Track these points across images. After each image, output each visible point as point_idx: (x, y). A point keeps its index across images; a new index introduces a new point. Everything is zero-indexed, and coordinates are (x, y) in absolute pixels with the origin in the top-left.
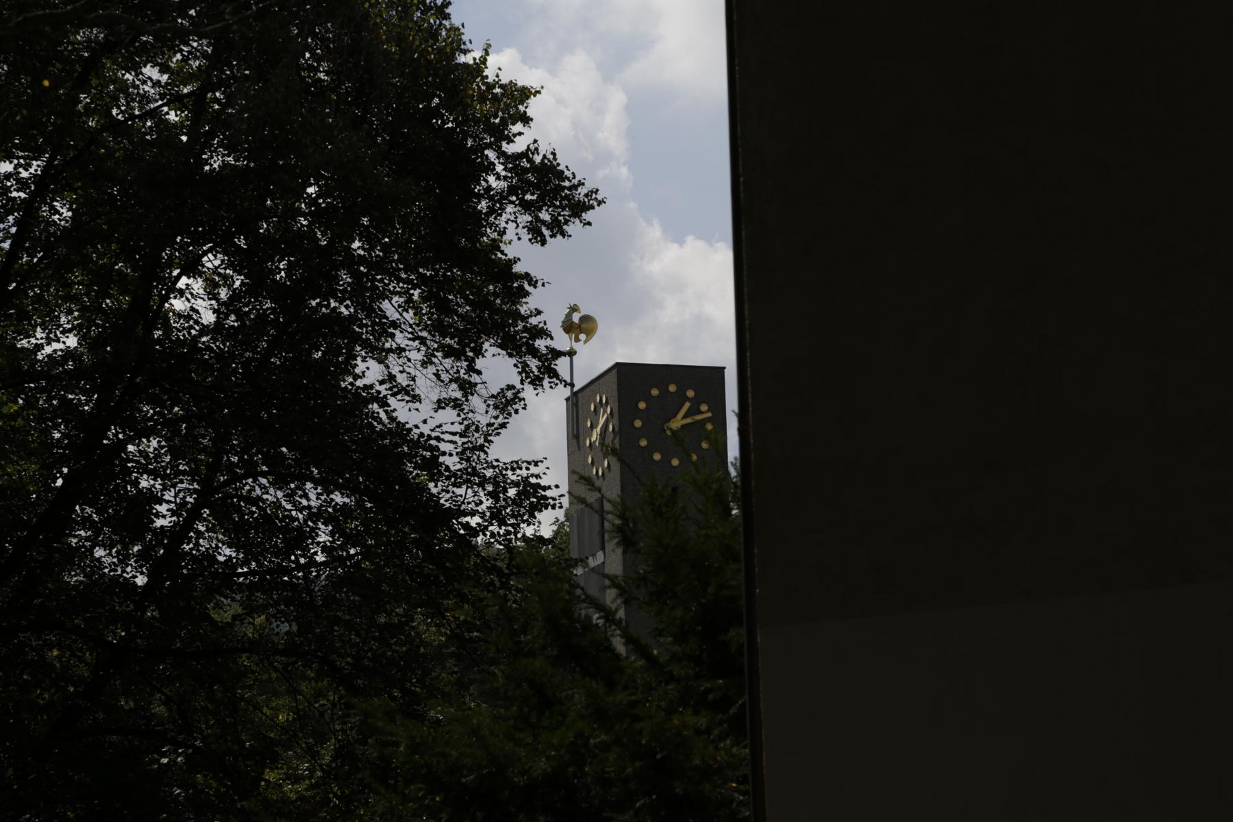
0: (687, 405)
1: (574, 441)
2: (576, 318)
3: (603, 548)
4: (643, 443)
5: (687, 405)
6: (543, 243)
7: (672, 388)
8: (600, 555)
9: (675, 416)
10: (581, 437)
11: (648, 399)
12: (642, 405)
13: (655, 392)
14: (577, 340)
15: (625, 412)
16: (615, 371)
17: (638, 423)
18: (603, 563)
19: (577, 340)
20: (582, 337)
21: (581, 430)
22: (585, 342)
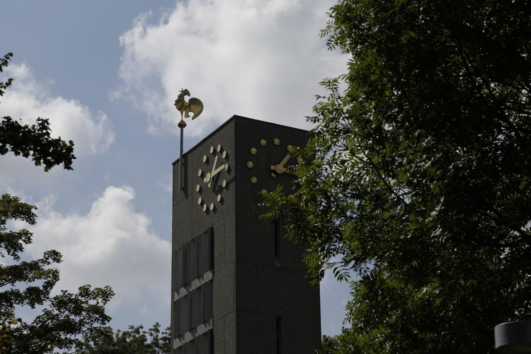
0: (288, 157)
1: (182, 193)
2: (187, 99)
3: (212, 267)
4: (254, 180)
5: (288, 157)
6: (9, 254)
7: (277, 141)
8: (208, 276)
9: (279, 163)
10: (190, 187)
11: (258, 146)
12: (254, 151)
13: (263, 142)
14: (187, 116)
15: (241, 154)
16: (233, 122)
17: (250, 164)
18: (211, 281)
19: (187, 116)
20: (191, 114)
21: (190, 181)
22: (193, 118)
